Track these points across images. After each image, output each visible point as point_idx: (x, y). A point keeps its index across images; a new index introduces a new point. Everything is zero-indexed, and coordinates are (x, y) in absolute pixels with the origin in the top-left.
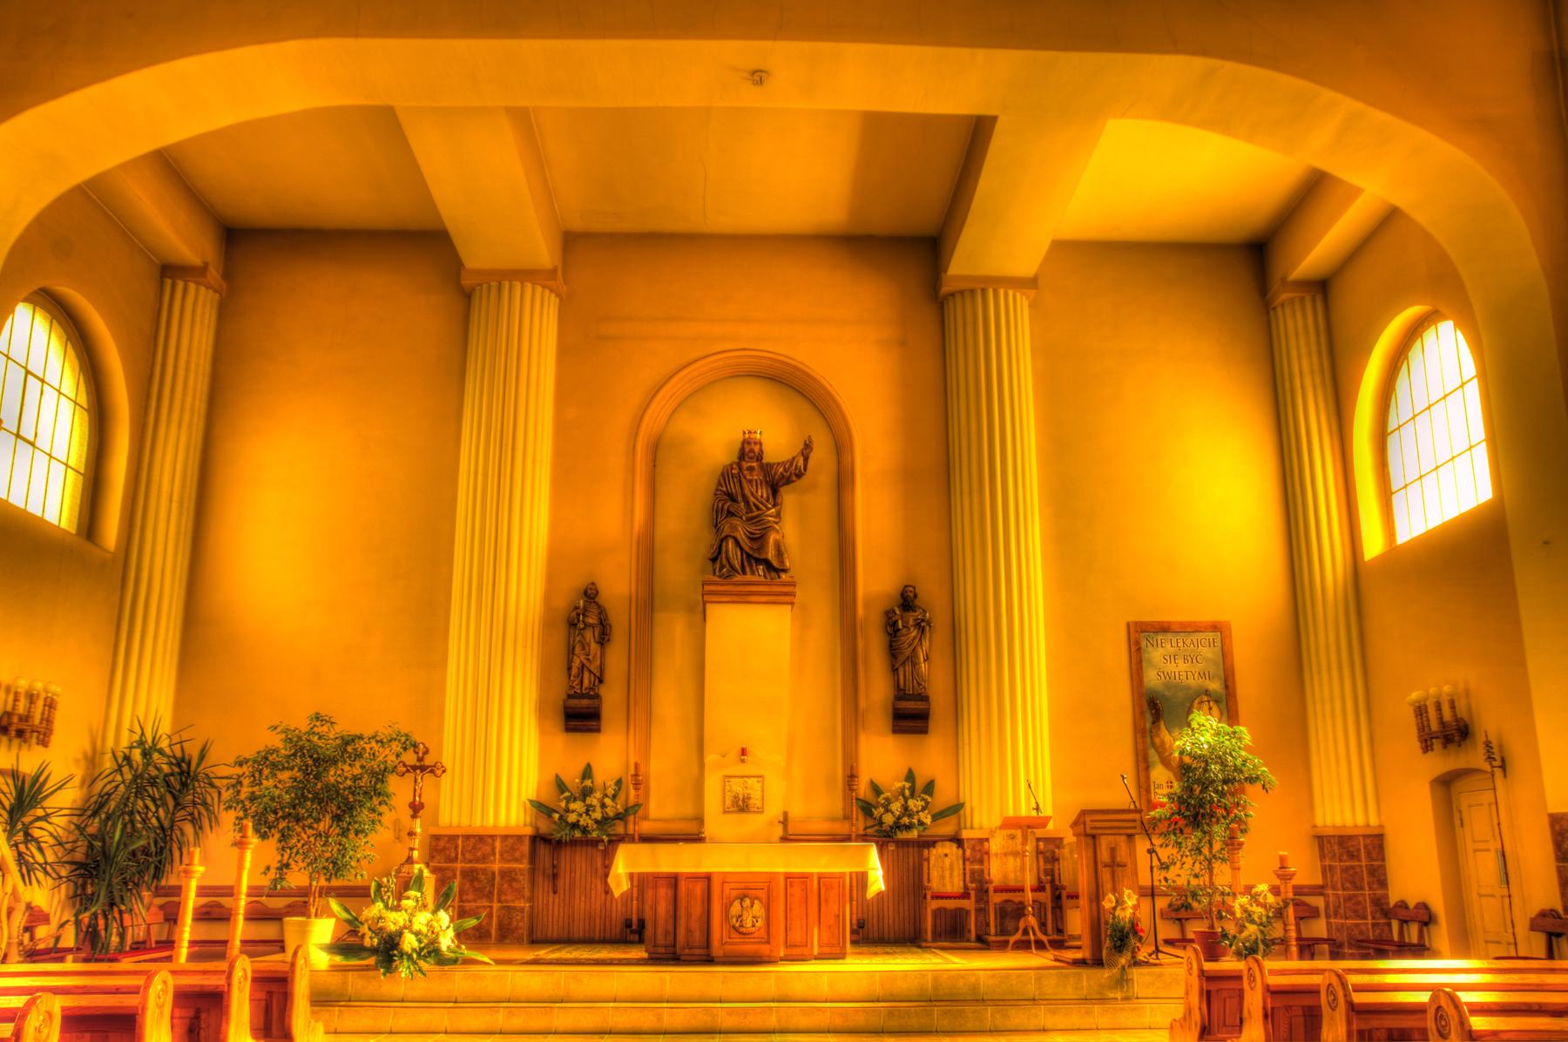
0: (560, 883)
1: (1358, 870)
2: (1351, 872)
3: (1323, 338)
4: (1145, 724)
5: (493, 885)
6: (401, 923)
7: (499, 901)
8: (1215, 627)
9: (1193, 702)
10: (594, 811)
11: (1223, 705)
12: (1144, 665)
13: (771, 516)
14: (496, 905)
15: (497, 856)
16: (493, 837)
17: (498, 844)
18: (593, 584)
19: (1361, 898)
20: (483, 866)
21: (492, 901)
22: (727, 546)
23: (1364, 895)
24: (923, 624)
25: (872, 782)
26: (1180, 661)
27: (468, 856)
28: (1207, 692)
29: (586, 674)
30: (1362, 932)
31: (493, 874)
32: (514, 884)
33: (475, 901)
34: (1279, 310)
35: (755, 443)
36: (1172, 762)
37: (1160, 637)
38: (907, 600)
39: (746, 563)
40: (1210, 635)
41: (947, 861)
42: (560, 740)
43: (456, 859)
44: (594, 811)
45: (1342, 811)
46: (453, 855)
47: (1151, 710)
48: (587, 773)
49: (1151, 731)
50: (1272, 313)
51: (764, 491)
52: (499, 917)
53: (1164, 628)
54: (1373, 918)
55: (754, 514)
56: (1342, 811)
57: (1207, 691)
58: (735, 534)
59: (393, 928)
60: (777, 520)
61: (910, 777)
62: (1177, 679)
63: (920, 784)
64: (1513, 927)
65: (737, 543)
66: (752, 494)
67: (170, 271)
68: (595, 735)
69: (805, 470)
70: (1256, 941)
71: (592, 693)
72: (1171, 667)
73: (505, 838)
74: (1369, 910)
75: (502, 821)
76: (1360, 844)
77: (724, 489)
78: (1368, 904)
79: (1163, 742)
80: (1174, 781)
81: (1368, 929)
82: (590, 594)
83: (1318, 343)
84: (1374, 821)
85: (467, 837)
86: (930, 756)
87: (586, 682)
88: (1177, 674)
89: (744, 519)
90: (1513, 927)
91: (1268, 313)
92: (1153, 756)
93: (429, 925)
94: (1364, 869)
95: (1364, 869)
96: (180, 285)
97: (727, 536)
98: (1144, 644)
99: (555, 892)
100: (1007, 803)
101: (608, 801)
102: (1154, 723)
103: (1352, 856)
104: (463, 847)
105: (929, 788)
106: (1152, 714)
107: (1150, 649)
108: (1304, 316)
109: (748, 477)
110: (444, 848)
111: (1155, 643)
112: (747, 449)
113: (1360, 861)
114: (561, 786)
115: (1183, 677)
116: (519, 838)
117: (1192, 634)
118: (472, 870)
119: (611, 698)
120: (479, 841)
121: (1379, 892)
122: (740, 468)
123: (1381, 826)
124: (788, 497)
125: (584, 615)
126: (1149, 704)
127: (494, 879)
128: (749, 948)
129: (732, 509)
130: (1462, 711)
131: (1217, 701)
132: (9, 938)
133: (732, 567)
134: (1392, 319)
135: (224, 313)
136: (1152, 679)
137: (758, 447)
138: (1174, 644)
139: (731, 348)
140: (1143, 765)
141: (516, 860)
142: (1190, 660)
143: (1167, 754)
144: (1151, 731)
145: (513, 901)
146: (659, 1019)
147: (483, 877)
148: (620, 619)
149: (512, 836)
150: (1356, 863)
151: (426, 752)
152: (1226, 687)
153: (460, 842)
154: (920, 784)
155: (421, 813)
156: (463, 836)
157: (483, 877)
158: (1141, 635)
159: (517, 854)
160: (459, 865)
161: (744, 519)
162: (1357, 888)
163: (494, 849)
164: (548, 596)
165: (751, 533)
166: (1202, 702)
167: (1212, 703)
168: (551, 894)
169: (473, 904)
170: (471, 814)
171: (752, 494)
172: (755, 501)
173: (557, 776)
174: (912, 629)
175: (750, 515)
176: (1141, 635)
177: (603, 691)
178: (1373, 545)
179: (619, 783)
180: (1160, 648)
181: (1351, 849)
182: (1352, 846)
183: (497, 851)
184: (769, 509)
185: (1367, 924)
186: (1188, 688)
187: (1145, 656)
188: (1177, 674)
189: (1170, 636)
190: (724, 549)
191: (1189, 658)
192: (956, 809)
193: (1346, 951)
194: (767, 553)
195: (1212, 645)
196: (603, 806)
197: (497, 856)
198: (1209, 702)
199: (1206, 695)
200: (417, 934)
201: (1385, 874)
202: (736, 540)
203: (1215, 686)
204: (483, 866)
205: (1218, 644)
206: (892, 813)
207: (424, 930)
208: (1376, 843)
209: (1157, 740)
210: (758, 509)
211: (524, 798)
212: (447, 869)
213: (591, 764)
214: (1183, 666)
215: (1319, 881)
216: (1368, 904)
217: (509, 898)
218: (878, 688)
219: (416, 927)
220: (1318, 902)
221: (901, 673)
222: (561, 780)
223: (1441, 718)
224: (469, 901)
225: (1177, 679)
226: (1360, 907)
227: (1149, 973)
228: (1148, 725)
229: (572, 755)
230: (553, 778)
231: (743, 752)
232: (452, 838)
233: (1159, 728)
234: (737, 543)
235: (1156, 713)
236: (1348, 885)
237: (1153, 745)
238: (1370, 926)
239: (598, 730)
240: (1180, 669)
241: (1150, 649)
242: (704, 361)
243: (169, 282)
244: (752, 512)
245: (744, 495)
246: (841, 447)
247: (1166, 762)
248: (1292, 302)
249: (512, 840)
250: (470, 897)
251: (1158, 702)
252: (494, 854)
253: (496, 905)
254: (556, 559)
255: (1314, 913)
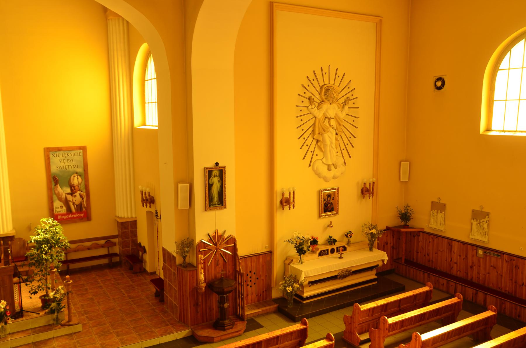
3: (126, 36)
4: (51, 186)
8: (80, 148)
9: (71, 177)
12: (51, 164)
28: (76, 173)
34: (110, 21)
36: (63, 199)
37: (58, 153)
40: (78, 151)
47: (54, 181)
50: (108, 20)
53: (59, 149)
54: (132, 247)
62: (65, 168)
64: (159, 267)
74: (130, 245)
78: (130, 243)
83: (124, 38)
84: (134, 216)
90: (159, 267)
91: (107, 20)
92: (55, 197)
98: (51, 156)
102: (55, 185)
103: (125, 228)
108: (119, 26)
111: (56, 156)
115: (67, 168)
117: (71, 151)
121: (134, 239)
123: (136, 217)
130: (151, 195)
131: (80, 176)
134: (140, 48)
136: (54, 169)
138: (64, 155)
142: (70, 161)
143: (60, 196)
150: (127, 230)
152: (84, 170)
167: (78, 177)
178: (137, 123)
187: (51, 161)
189: (62, 152)
191: (70, 161)
195: (79, 155)
198: (77, 176)
199: (76, 173)
201: (137, 233)
205: (82, 154)
208: (134, 224)
215: (117, 234)
216: (130, 243)
220: (116, 240)
223: (146, 197)
225: (65, 168)
228: (53, 186)
233: (57, 187)
235: (56, 182)
240: (65, 165)
248: (111, 19)
251: (57, 177)
255: (114, 244)
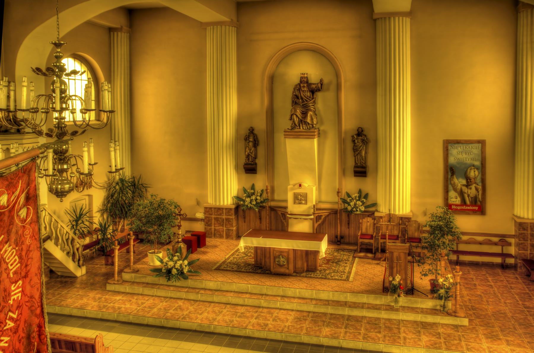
0: (246, 220)
1: (526, 234)
2: (523, 235)
5: (223, 223)
6: (172, 266)
7: (226, 227)
8: (479, 142)
9: (468, 169)
10: (253, 201)
11: (480, 170)
13: (311, 103)
14: (225, 228)
15: (224, 214)
16: (223, 209)
17: (224, 210)
18: (251, 127)
19: (526, 244)
20: (220, 217)
21: (223, 227)
22: (293, 117)
23: (528, 243)
24: (364, 142)
25: (347, 192)
26: (464, 154)
27: (215, 213)
28: (473, 166)
29: (250, 157)
30: (525, 256)
31: (223, 219)
32: (230, 222)
33: (218, 227)
35: (305, 78)
36: (458, 190)
37: (456, 145)
38: (360, 133)
39: (300, 123)
40: (477, 145)
41: (369, 224)
42: (244, 176)
43: (212, 214)
44: (253, 201)
45: (524, 212)
46: (211, 213)
48: (253, 187)
49: (450, 179)
51: (309, 94)
52: (226, 232)
53: (458, 142)
54: (531, 251)
55: (305, 103)
56: (524, 212)
57: (474, 165)
58: (296, 113)
59: (169, 267)
60: (313, 104)
61: (360, 192)
63: (363, 195)
65: (297, 116)
66: (304, 96)
67: (111, 30)
68: (255, 175)
69: (321, 88)
70: (446, 291)
71: (252, 163)
72: (460, 156)
73: (226, 209)
74: (529, 248)
75: (226, 203)
76: (528, 226)
77: (295, 94)
79: (454, 183)
80: (458, 196)
81: (528, 255)
82: (252, 131)
85: (215, 208)
86: (366, 185)
87: (250, 160)
88: (462, 159)
89: (301, 105)
92: (450, 187)
93: (181, 265)
94: (529, 234)
95: (529, 234)
96: (116, 33)
97: (293, 114)
98: (449, 147)
99: (245, 222)
100: (391, 205)
101: (258, 198)
102: (451, 176)
103: (524, 229)
104: (214, 211)
105: (366, 196)
106: (451, 173)
107: (452, 149)
109: (303, 89)
110: (209, 211)
112: (302, 80)
113: (528, 231)
114: (245, 191)
116: (231, 209)
118: (217, 218)
119: (260, 162)
120: (219, 210)
122: (300, 86)
124: (319, 96)
125: (248, 138)
126: (450, 170)
127: (224, 220)
128: (282, 270)
129: (297, 102)
131: (477, 169)
132: (79, 254)
133: (295, 124)
135: (131, 39)
136: (452, 160)
137: (306, 79)
139: (296, 42)
140: (446, 191)
141: (231, 215)
142: (468, 154)
144: (450, 179)
145: (230, 227)
146: (244, 301)
147: (220, 220)
148: (262, 138)
149: (228, 208)
151: (181, 210)
152: (482, 164)
153: (213, 209)
154: (363, 195)
155: (181, 228)
156: (214, 208)
157: (220, 220)
158: (448, 144)
159: (230, 214)
160: (213, 216)
161: (301, 105)
162: (525, 241)
163: (223, 212)
164: (237, 131)
165: (303, 111)
166: (471, 169)
167: (475, 170)
168: (243, 223)
169: (218, 228)
170: (216, 201)
171: (304, 96)
172: (305, 98)
173: (243, 187)
174: (360, 143)
175: (303, 103)
176: (448, 144)
177: (257, 161)
179: (262, 191)
180: (456, 149)
181: (524, 227)
182: (525, 226)
183: (224, 212)
184: (310, 100)
185: (527, 253)
186: (466, 164)
187: (450, 152)
188: (462, 159)
189: (460, 145)
190: (292, 118)
192: (375, 205)
193: (529, 252)
194: (307, 119)
195: (477, 148)
196: (256, 199)
197: (224, 214)
198: (474, 169)
200: (176, 269)
202: (296, 115)
203: (477, 163)
204: (220, 217)
206: (351, 206)
207: (179, 268)
209: (452, 182)
210: (307, 101)
211: (232, 196)
212: (210, 217)
213: (255, 184)
214: (464, 156)
217: (228, 226)
218: (350, 162)
219: (176, 267)
221: (356, 157)
222: (245, 189)
224: (217, 227)
225: (462, 160)
226: (526, 247)
227: (406, 299)
228: (449, 177)
229: (248, 180)
230: (242, 188)
231: (300, 185)
232: (211, 208)
233: (453, 178)
234: (297, 116)
236: (521, 239)
237: (451, 184)
238: (529, 254)
239: (256, 173)
241: (452, 149)
242: (288, 47)
243: (112, 33)
244: (304, 102)
245: (301, 96)
246: (337, 75)
247: (455, 190)
249: (228, 210)
250: (217, 226)
252: (223, 213)
253: (225, 228)
254: (240, 120)
